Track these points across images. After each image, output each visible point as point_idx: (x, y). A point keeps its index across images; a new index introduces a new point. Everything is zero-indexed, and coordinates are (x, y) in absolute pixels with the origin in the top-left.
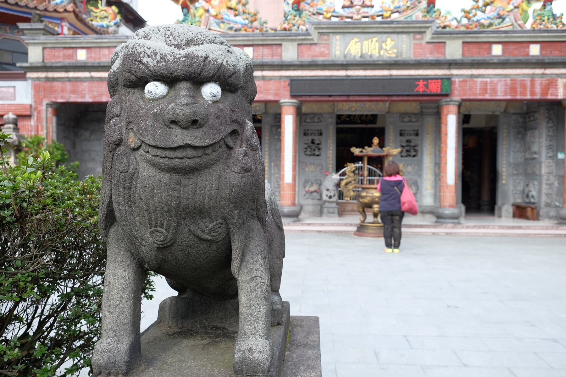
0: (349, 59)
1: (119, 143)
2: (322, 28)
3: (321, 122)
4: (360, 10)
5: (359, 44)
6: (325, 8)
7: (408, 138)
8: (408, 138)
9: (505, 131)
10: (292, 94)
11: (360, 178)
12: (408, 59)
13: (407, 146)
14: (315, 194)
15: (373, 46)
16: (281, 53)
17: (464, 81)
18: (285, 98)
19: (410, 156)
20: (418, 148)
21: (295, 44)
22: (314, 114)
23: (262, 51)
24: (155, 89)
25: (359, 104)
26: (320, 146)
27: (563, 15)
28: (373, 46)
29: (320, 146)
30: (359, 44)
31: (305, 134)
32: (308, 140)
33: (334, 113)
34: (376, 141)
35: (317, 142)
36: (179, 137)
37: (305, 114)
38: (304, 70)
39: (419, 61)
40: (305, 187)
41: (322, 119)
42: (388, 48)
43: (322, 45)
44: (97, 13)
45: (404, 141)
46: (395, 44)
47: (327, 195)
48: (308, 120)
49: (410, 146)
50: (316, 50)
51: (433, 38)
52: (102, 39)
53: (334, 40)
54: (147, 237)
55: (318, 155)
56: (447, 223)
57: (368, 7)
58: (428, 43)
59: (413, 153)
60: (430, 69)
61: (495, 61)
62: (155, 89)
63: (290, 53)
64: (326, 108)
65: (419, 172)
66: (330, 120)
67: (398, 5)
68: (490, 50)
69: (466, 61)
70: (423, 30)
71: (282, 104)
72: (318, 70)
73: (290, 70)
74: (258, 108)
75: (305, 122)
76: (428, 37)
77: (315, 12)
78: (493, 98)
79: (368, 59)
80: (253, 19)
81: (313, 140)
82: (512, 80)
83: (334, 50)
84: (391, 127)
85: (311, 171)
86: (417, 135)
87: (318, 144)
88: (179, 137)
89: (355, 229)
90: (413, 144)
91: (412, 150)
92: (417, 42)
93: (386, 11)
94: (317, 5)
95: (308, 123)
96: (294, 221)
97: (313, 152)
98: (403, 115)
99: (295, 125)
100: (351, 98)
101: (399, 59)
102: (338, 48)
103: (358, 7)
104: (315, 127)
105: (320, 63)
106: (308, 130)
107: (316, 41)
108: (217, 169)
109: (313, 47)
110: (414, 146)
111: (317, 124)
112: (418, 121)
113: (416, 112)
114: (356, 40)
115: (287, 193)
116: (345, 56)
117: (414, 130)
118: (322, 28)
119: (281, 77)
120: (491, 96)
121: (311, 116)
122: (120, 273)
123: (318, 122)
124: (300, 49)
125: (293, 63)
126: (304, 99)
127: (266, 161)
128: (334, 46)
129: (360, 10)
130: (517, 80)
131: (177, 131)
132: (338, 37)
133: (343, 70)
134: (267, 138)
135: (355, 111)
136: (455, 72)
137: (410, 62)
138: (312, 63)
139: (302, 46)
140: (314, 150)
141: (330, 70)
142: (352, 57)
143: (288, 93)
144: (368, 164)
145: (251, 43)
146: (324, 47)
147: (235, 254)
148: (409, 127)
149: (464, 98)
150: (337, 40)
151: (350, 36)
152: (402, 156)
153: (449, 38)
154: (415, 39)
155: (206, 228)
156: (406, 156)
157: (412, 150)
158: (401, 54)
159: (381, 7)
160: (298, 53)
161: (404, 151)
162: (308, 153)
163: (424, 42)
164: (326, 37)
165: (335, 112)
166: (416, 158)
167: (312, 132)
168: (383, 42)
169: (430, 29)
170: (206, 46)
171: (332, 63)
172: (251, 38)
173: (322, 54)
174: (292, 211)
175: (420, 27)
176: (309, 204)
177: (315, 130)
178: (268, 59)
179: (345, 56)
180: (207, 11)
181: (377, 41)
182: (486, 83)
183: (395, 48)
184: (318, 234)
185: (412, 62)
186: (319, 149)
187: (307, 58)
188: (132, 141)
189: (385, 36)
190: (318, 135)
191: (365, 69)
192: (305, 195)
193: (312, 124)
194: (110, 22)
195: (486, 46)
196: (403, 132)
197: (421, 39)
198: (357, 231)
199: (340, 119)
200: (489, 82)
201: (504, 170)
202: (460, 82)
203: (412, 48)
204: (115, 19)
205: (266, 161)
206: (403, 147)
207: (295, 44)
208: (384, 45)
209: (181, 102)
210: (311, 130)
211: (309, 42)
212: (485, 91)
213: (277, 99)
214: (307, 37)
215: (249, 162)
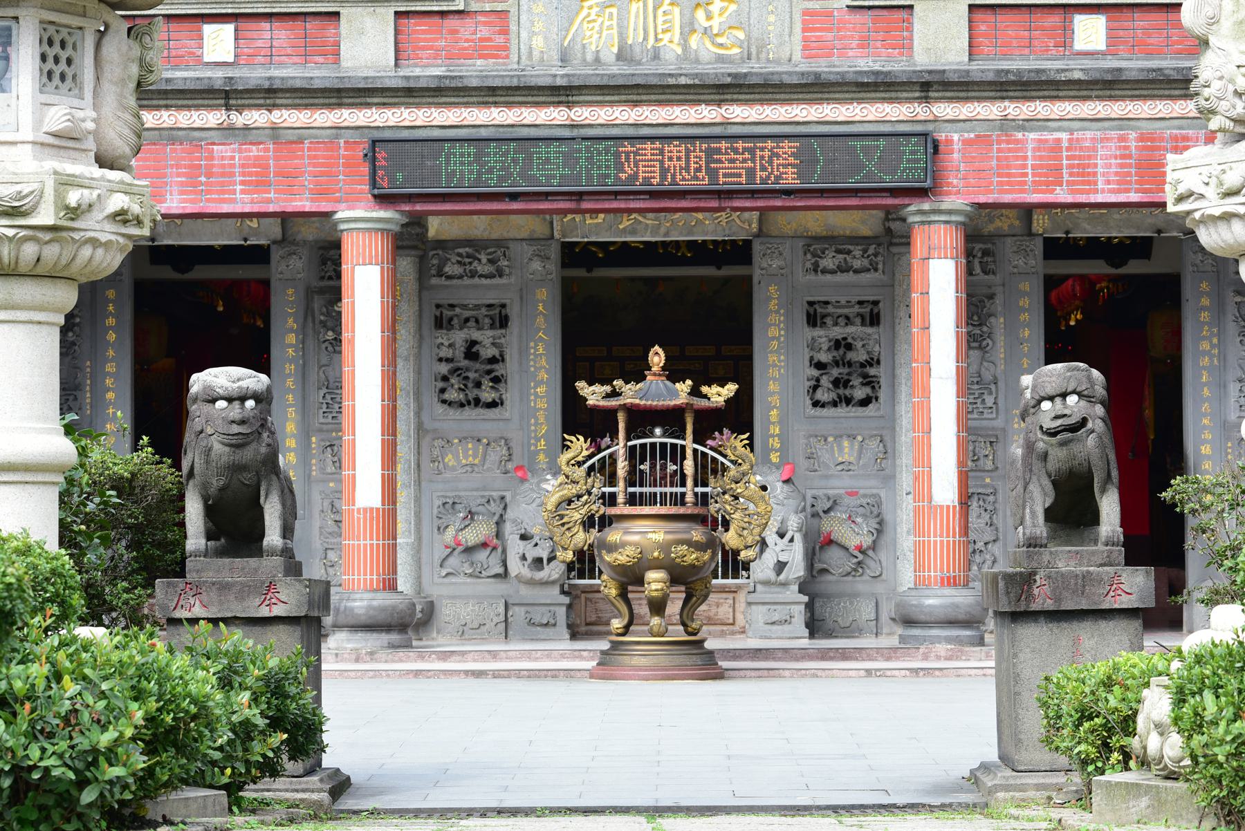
1: (201, 432)
7: (838, 332)
9: (1205, 301)
10: (376, 192)
11: (637, 490)
13: (837, 364)
14: (482, 555)
16: (338, 44)
17: (982, 141)
19: (848, 401)
23: (267, 35)
24: (221, 404)
26: (499, 370)
28: (660, 19)
29: (499, 370)
31: (439, 323)
34: (656, 359)
35: (488, 352)
36: (236, 429)
37: (441, 244)
38: (418, 106)
40: (441, 530)
42: (715, 24)
46: (738, 13)
47: (524, 558)
49: (850, 364)
54: (214, 482)
55: (493, 405)
56: (934, 640)
59: (860, 393)
61: (1077, 75)
62: (221, 404)
64: (521, 225)
66: (536, 265)
68: (1065, 36)
69: (977, 77)
71: (342, 227)
73: (368, 105)
75: (440, 274)
78: (1082, 199)
81: (474, 343)
82: (1141, 138)
85: (466, 465)
87: (493, 360)
88: (236, 429)
91: (856, 381)
95: (449, 277)
96: (392, 646)
98: (816, 244)
100: (586, 205)
104: (478, 293)
105: (474, 83)
106: (452, 306)
108: (254, 445)
110: (862, 365)
115: (361, 544)
120: (1073, 192)
122: (196, 505)
123: (490, 276)
127: (291, 427)
130: (1162, 139)
131: (235, 426)
134: (291, 338)
136: (945, 109)
137: (787, 80)
138: (447, 83)
140: (478, 385)
142: (590, 57)
144: (695, 441)
147: (262, 493)
148: (843, 288)
149: (982, 199)
152: (816, 404)
155: (247, 478)
156: (835, 404)
157: (856, 381)
161: (825, 381)
162: (452, 395)
165: (557, 235)
166: (871, 409)
167: (467, 314)
170: (248, 381)
174: (383, 609)
177: (477, 307)
178: (290, 72)
182: (1056, 147)
184: (472, 681)
186: (496, 380)
187: (426, 70)
188: (209, 430)
193: (467, 281)
195: (1054, 19)
199: (576, 255)
200: (1065, 144)
201: (1206, 450)
202: (966, 142)
203: (798, 27)
205: (291, 427)
206: (820, 366)
208: (700, 14)
209: (235, 411)
210: (464, 307)
212: (1053, 175)
213: (324, 207)
215: (270, 441)
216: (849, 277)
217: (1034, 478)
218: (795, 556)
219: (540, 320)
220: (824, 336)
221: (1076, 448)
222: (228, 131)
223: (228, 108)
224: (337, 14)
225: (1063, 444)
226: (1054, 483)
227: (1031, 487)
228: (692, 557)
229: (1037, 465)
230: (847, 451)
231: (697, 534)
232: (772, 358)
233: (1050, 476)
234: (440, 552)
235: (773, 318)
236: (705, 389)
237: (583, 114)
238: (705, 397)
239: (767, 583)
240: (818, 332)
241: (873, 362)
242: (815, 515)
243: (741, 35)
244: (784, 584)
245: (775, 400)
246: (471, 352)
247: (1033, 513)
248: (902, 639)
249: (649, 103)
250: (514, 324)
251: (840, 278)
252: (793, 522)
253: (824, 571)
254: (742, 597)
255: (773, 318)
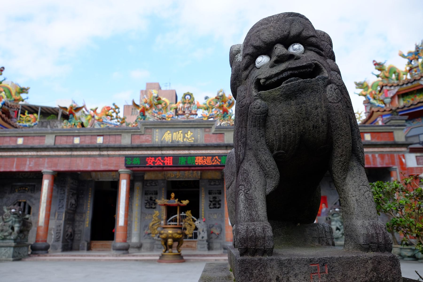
0: (164, 144)
2: (147, 125)
3: (156, 185)
4: (188, 116)
5: (171, 134)
6: (167, 116)
7: (214, 195)
8: (214, 195)
12: (201, 143)
13: (214, 201)
15: (179, 136)
18: (121, 169)
20: (221, 202)
21: (130, 134)
22: (152, 181)
25: (182, 172)
27: (29, 88)
28: (179, 136)
30: (171, 134)
32: (148, 198)
33: (165, 179)
35: (154, 199)
37: (147, 181)
38: (134, 150)
39: (207, 145)
40: (144, 230)
41: (157, 184)
42: (189, 137)
43: (147, 135)
44: (22, 118)
45: (212, 197)
48: (148, 185)
49: (216, 201)
50: (144, 138)
51: (216, 131)
52: (6, 131)
53: (155, 132)
57: (193, 114)
58: (213, 134)
59: (218, 206)
60: (215, 149)
63: (126, 140)
64: (160, 176)
65: (222, 219)
66: (163, 184)
67: (212, 114)
70: (210, 126)
72: (143, 150)
73: (125, 150)
74: (115, 177)
75: (146, 185)
76: (213, 130)
77: (161, 118)
79: (176, 143)
80: (122, 122)
83: (154, 138)
84: (203, 188)
86: (220, 193)
89: (158, 258)
90: (217, 200)
91: (217, 204)
92: (207, 133)
93: (205, 117)
94: (162, 114)
97: (151, 206)
98: (211, 180)
99: (128, 186)
101: (196, 143)
102: (157, 137)
103: (187, 115)
105: (144, 146)
107: (143, 133)
109: (141, 136)
111: (154, 187)
112: (220, 184)
113: (218, 178)
114: (168, 132)
116: (162, 142)
117: (218, 191)
118: (147, 125)
119: (120, 155)
121: (150, 181)
123: (154, 186)
124: (133, 138)
125: (127, 146)
126: (134, 169)
128: (154, 135)
129: (188, 116)
132: (157, 130)
133: (160, 150)
135: (179, 178)
137: (201, 145)
139: (135, 136)
140: (152, 205)
141: (151, 150)
143: (123, 165)
145: (102, 134)
146: (148, 136)
150: (156, 132)
151: (165, 130)
152: (210, 208)
153: (226, 131)
154: (205, 131)
157: (217, 204)
158: (197, 141)
159: (202, 115)
160: (131, 140)
161: (212, 204)
162: (147, 206)
163: (211, 133)
164: (150, 130)
166: (220, 209)
168: (186, 133)
169: (214, 126)
171: (151, 146)
172: (102, 131)
173: (147, 141)
175: (208, 124)
176: (147, 243)
178: (112, 144)
179: (162, 142)
180: (93, 117)
181: (181, 133)
183: (193, 137)
185: (203, 145)
187: (137, 143)
189: (187, 130)
190: (155, 194)
191: (174, 150)
192: (144, 236)
194: (31, 123)
196: (211, 192)
197: (210, 131)
198: (160, 259)
204: (35, 122)
207: (130, 134)
208: (186, 135)
211: (139, 133)
214: (137, 130)
216: (216, 186)
217: (250, 154)
218: (205, 235)
219: (163, 194)
220: (211, 196)
221: (310, 101)
222: (100, 155)
223: (100, 151)
224: (121, 135)
225: (290, 95)
226: (276, 158)
227: (246, 166)
228: (178, 236)
229: (254, 134)
230: (215, 216)
231: (179, 231)
232: (203, 200)
233: (272, 151)
234: (144, 234)
235: (203, 193)
236: (182, 201)
237: (164, 152)
238: (182, 203)
239: (200, 240)
240: (211, 196)
241: (220, 201)
242: (210, 228)
243: (193, 139)
244: (203, 241)
245: (203, 207)
246: (151, 199)
247: (249, 200)
248: (224, 252)
249: (176, 150)
250: (158, 195)
251: (214, 186)
252: (205, 229)
253: (211, 238)
254: (197, 242)
255: (203, 193)
